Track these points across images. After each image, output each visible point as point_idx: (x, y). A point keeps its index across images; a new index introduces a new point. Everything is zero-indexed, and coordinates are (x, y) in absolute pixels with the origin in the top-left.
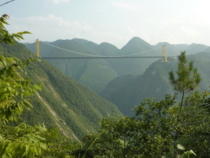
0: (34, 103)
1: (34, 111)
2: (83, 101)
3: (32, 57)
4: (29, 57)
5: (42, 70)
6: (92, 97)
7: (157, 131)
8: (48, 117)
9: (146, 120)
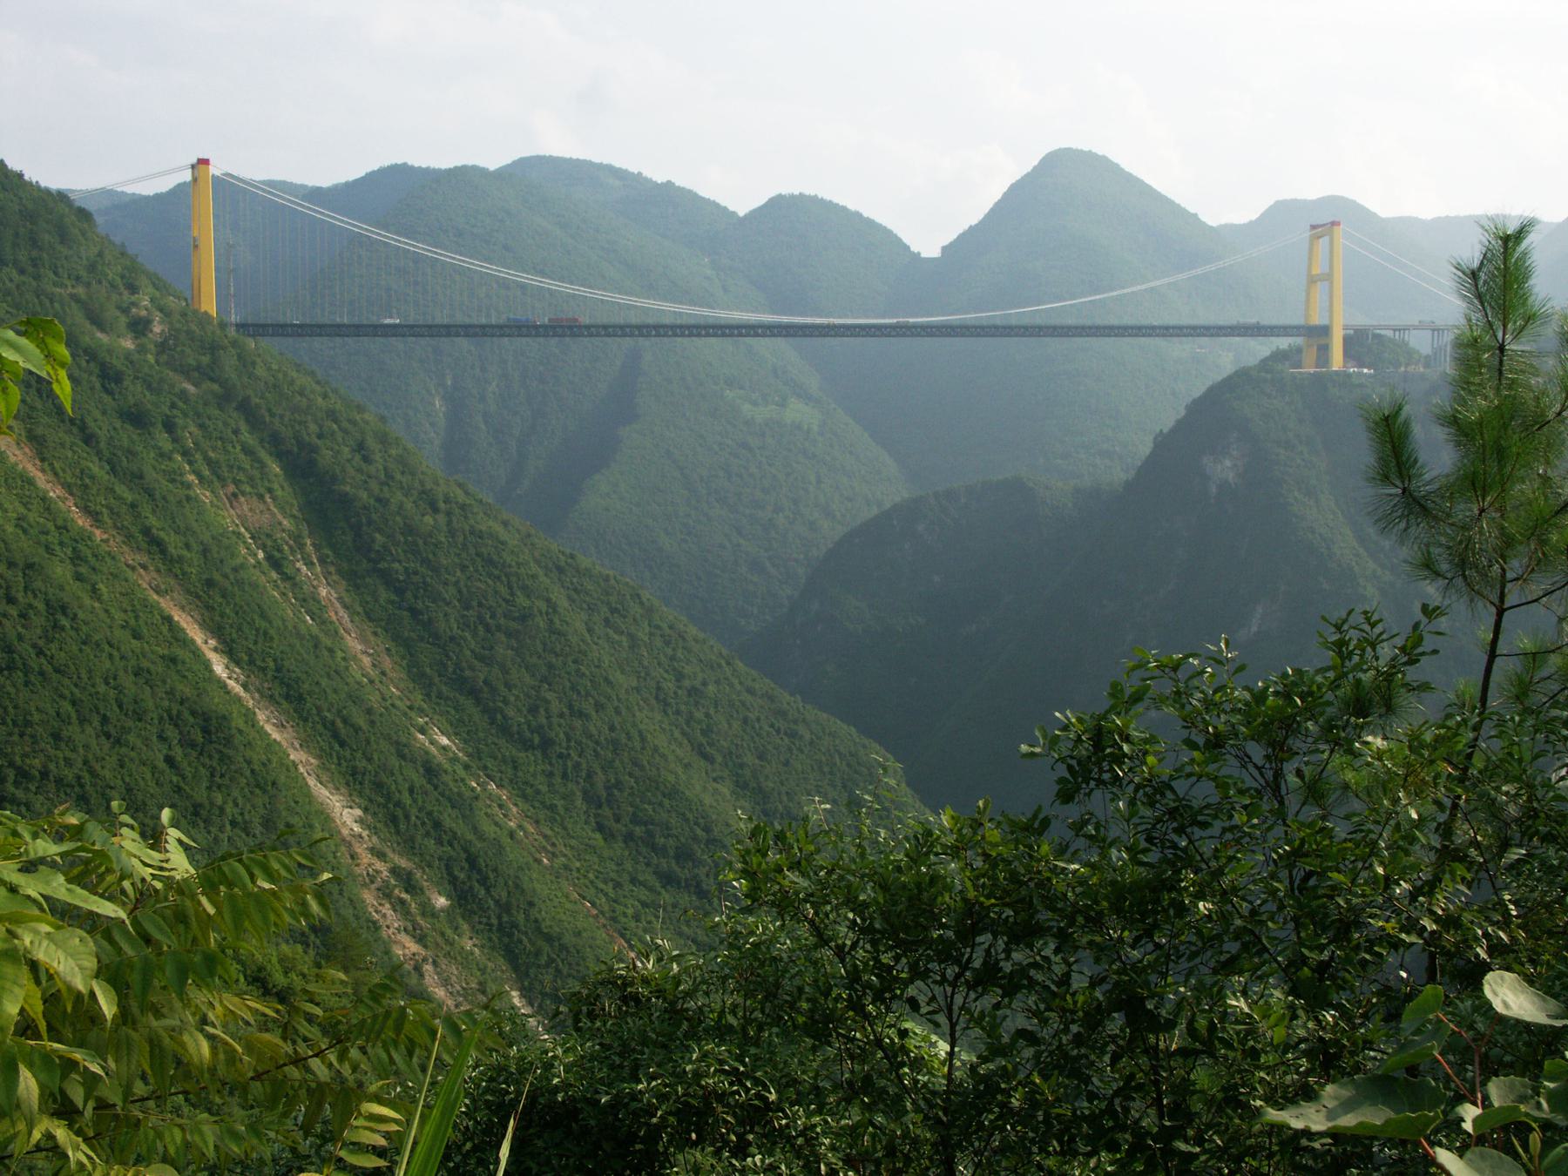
0: (175, 720)
2: (599, 707)
4: (125, 311)
5: (247, 436)
6: (680, 677)
7: (1252, 943)
9: (1149, 840)
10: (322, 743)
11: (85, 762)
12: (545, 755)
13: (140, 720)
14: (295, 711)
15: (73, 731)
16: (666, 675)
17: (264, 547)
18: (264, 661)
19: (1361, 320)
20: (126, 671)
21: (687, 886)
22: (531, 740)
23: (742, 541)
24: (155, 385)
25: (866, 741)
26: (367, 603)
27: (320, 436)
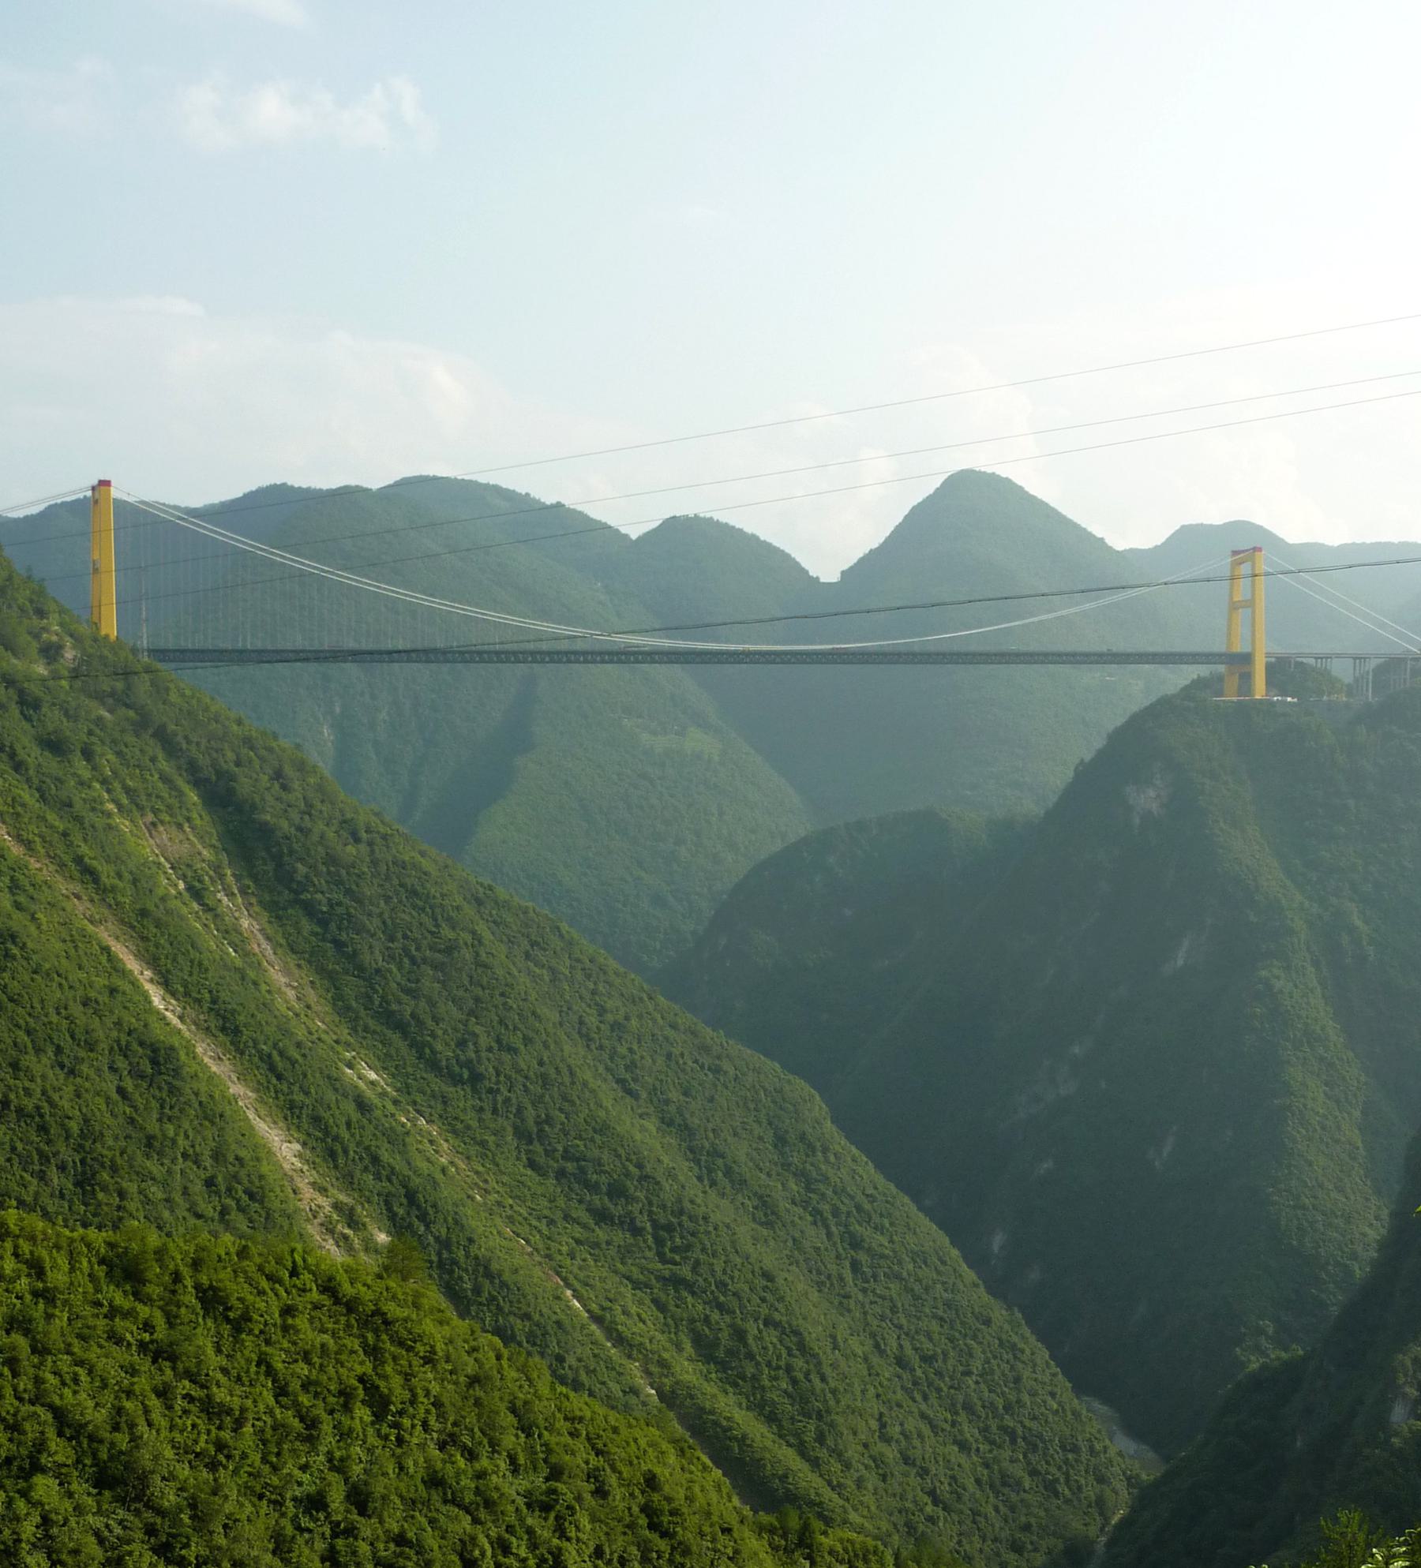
0: (125, 1052)
1: (121, 1120)
2: (527, 1041)
3: (68, 642)
4: (37, 636)
5: (164, 764)
6: (602, 1011)
8: (243, 1173)
10: (259, 1077)
11: (44, 1093)
12: (475, 1090)
13: (92, 1050)
14: (232, 1043)
15: (29, 1060)
16: (587, 1009)
17: (184, 877)
18: (199, 992)
19: (1279, 650)
20: (75, 1001)
21: (622, 1223)
22: (461, 1075)
23: (643, 874)
24: (71, 712)
25: (791, 1077)
26: (290, 935)
27: (238, 764)
